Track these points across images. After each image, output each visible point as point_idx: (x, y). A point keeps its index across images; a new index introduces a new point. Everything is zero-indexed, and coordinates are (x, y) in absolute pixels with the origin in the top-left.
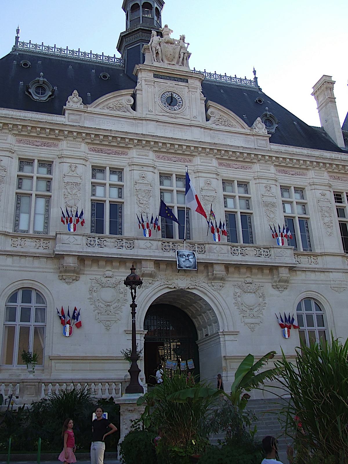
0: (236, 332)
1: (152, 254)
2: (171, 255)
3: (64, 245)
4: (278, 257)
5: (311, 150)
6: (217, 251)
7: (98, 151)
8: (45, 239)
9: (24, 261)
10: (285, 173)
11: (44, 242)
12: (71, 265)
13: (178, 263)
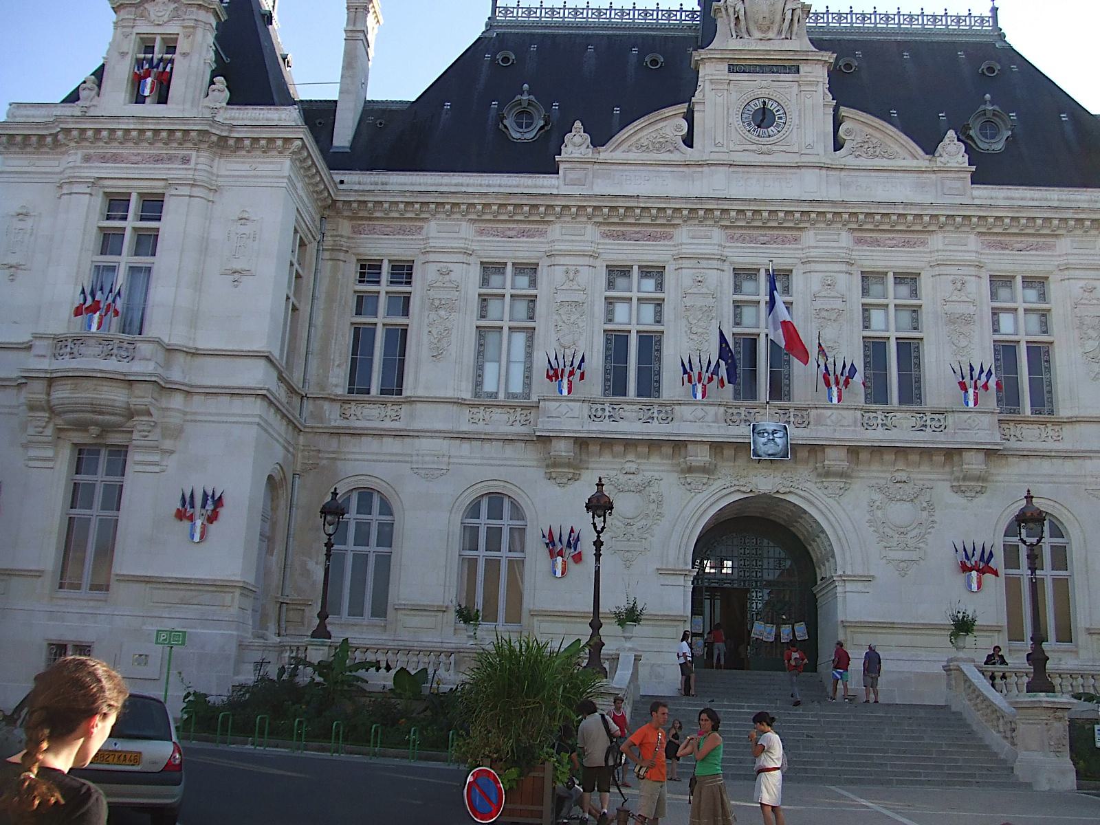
0: (867, 576)
1: (706, 432)
2: (741, 432)
3: (551, 419)
4: (960, 431)
5: (1070, 191)
6: (832, 422)
7: (618, 238)
8: (523, 408)
9: (491, 449)
10: (1003, 248)
12: (564, 454)
13: (752, 448)
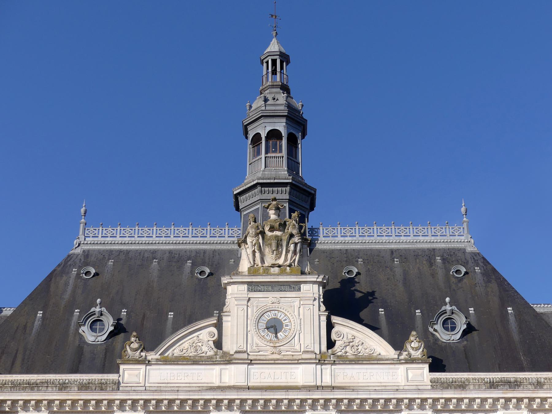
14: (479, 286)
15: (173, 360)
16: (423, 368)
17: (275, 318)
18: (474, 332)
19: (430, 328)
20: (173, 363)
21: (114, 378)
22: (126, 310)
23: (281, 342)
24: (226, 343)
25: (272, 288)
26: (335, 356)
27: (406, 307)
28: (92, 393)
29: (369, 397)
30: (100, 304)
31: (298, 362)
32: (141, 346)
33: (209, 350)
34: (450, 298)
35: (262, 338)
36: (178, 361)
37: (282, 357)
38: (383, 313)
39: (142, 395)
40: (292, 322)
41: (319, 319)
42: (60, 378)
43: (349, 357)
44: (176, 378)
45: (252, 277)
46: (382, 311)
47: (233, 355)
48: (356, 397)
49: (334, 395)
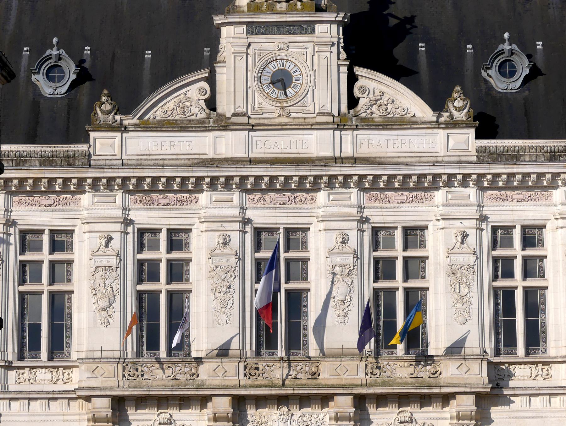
11: (64, 371)
14: (554, 8)
15: (155, 126)
16: (468, 134)
17: (282, 69)
18: (539, 77)
19: (483, 71)
20: (155, 129)
21: (83, 149)
22: (89, 48)
23: (290, 100)
24: (220, 102)
25: (279, 29)
26: (358, 119)
27: (454, 40)
28: (58, 171)
29: (399, 173)
30: (57, 44)
31: (311, 127)
32: (114, 107)
33: (200, 111)
34: (508, 32)
35: (267, 96)
36: (162, 127)
37: (292, 120)
38: (424, 49)
39: (119, 172)
40: (305, 75)
41: (339, 70)
42: (17, 149)
43: (375, 120)
44: (160, 148)
45: (253, 16)
46: (422, 47)
47: (229, 118)
48: (383, 172)
49: (355, 170)
